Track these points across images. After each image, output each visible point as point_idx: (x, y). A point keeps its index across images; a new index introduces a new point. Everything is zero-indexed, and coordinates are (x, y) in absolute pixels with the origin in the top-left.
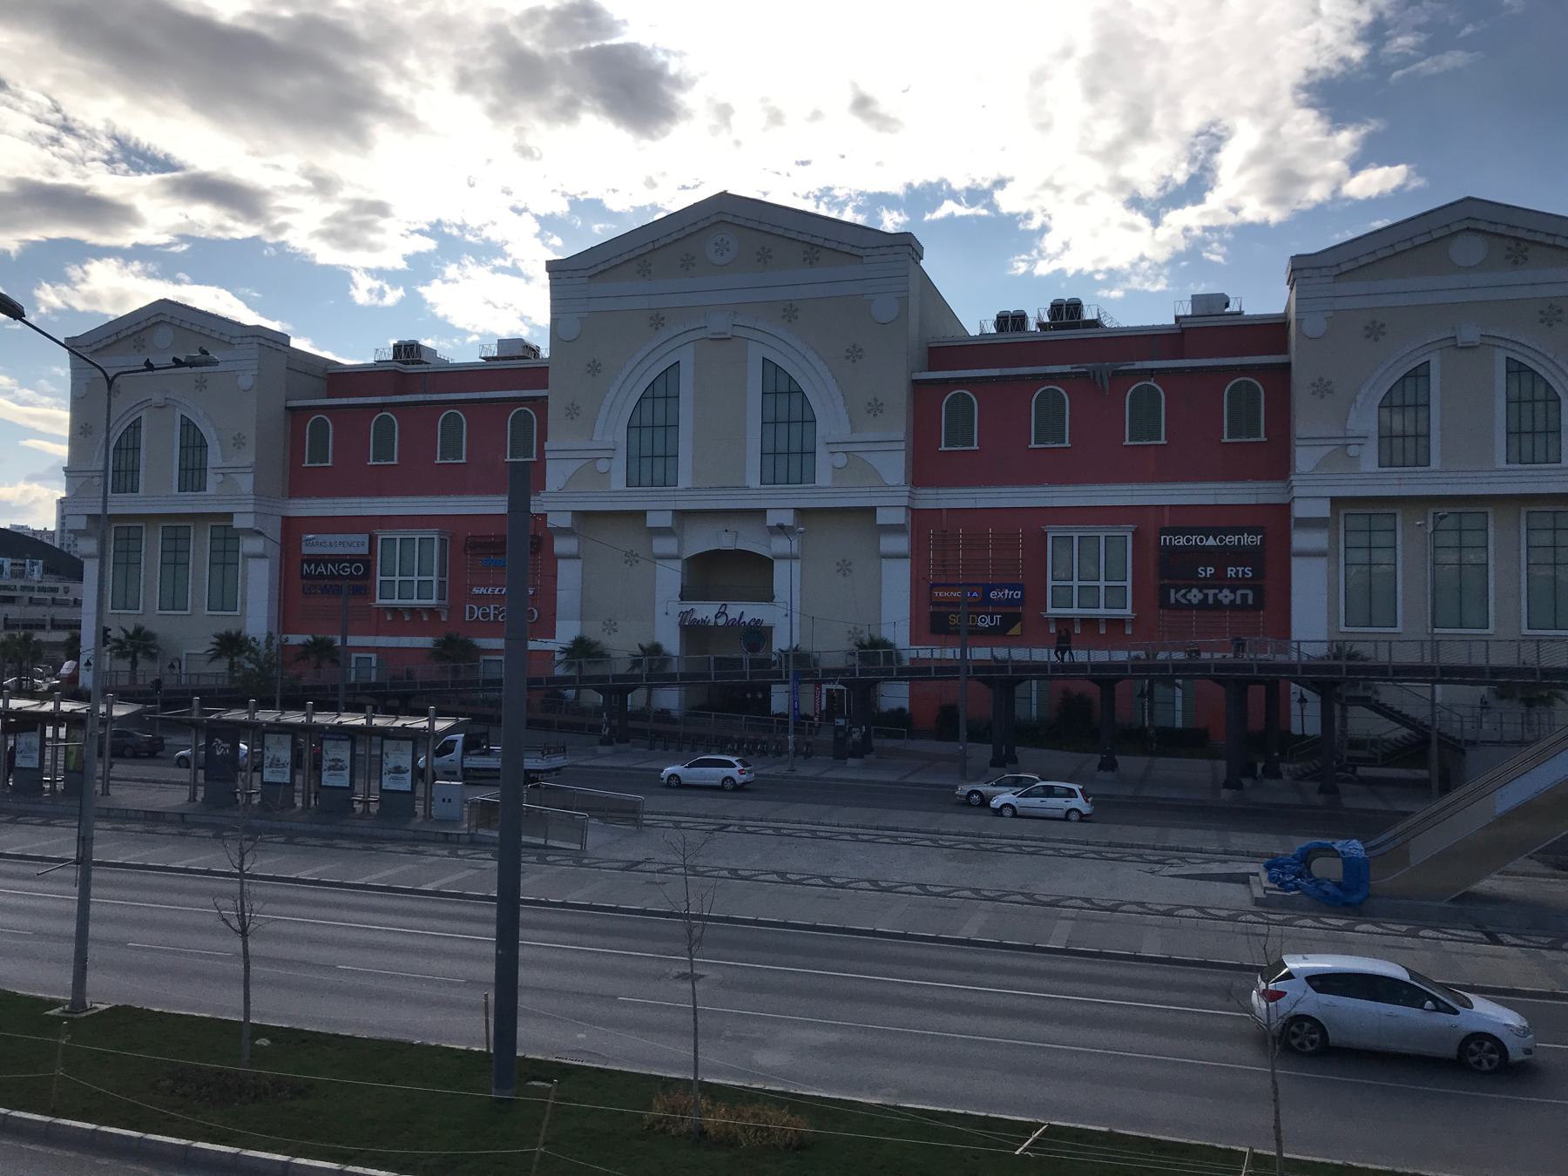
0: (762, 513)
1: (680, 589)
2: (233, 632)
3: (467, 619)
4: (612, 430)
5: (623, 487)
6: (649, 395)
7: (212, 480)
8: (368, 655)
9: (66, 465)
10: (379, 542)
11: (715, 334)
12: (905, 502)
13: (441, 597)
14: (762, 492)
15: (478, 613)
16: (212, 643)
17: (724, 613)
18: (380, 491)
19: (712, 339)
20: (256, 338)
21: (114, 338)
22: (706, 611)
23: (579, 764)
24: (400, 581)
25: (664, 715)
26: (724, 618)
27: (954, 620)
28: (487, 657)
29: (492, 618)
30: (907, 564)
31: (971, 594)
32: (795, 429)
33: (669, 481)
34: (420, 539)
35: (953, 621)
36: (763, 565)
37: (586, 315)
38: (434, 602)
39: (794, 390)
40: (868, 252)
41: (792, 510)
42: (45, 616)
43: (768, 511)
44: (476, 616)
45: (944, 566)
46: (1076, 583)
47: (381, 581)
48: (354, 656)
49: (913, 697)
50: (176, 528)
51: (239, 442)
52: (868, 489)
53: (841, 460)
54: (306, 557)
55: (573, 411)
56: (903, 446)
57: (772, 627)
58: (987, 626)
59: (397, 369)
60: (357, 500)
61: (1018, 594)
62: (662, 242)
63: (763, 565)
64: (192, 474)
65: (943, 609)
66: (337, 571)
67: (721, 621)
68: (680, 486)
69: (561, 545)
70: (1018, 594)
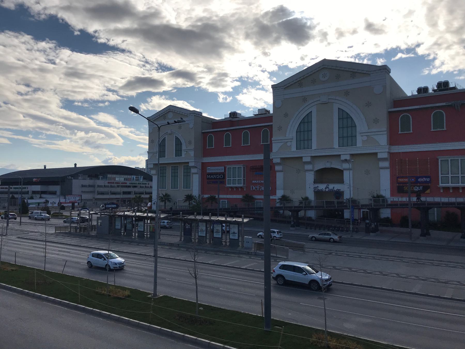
4: (291, 133)
6: (303, 122)
7: (183, 153)
9: (148, 151)
10: (227, 168)
11: (323, 102)
13: (244, 184)
15: (254, 188)
17: (328, 187)
21: (159, 116)
22: (322, 187)
24: (238, 179)
25: (310, 219)
27: (406, 188)
28: (257, 201)
29: (258, 190)
30: (389, 170)
31: (412, 180)
33: (309, 147)
36: (341, 172)
37: (283, 100)
38: (242, 185)
39: (349, 117)
42: (108, 190)
46: (232, 179)
49: (392, 214)
50: (175, 166)
51: (190, 143)
54: (208, 174)
55: (280, 128)
56: (386, 133)
58: (417, 190)
61: (428, 180)
62: (306, 76)
63: (341, 172)
64: (178, 152)
65: (402, 185)
67: (327, 190)
70: (428, 180)
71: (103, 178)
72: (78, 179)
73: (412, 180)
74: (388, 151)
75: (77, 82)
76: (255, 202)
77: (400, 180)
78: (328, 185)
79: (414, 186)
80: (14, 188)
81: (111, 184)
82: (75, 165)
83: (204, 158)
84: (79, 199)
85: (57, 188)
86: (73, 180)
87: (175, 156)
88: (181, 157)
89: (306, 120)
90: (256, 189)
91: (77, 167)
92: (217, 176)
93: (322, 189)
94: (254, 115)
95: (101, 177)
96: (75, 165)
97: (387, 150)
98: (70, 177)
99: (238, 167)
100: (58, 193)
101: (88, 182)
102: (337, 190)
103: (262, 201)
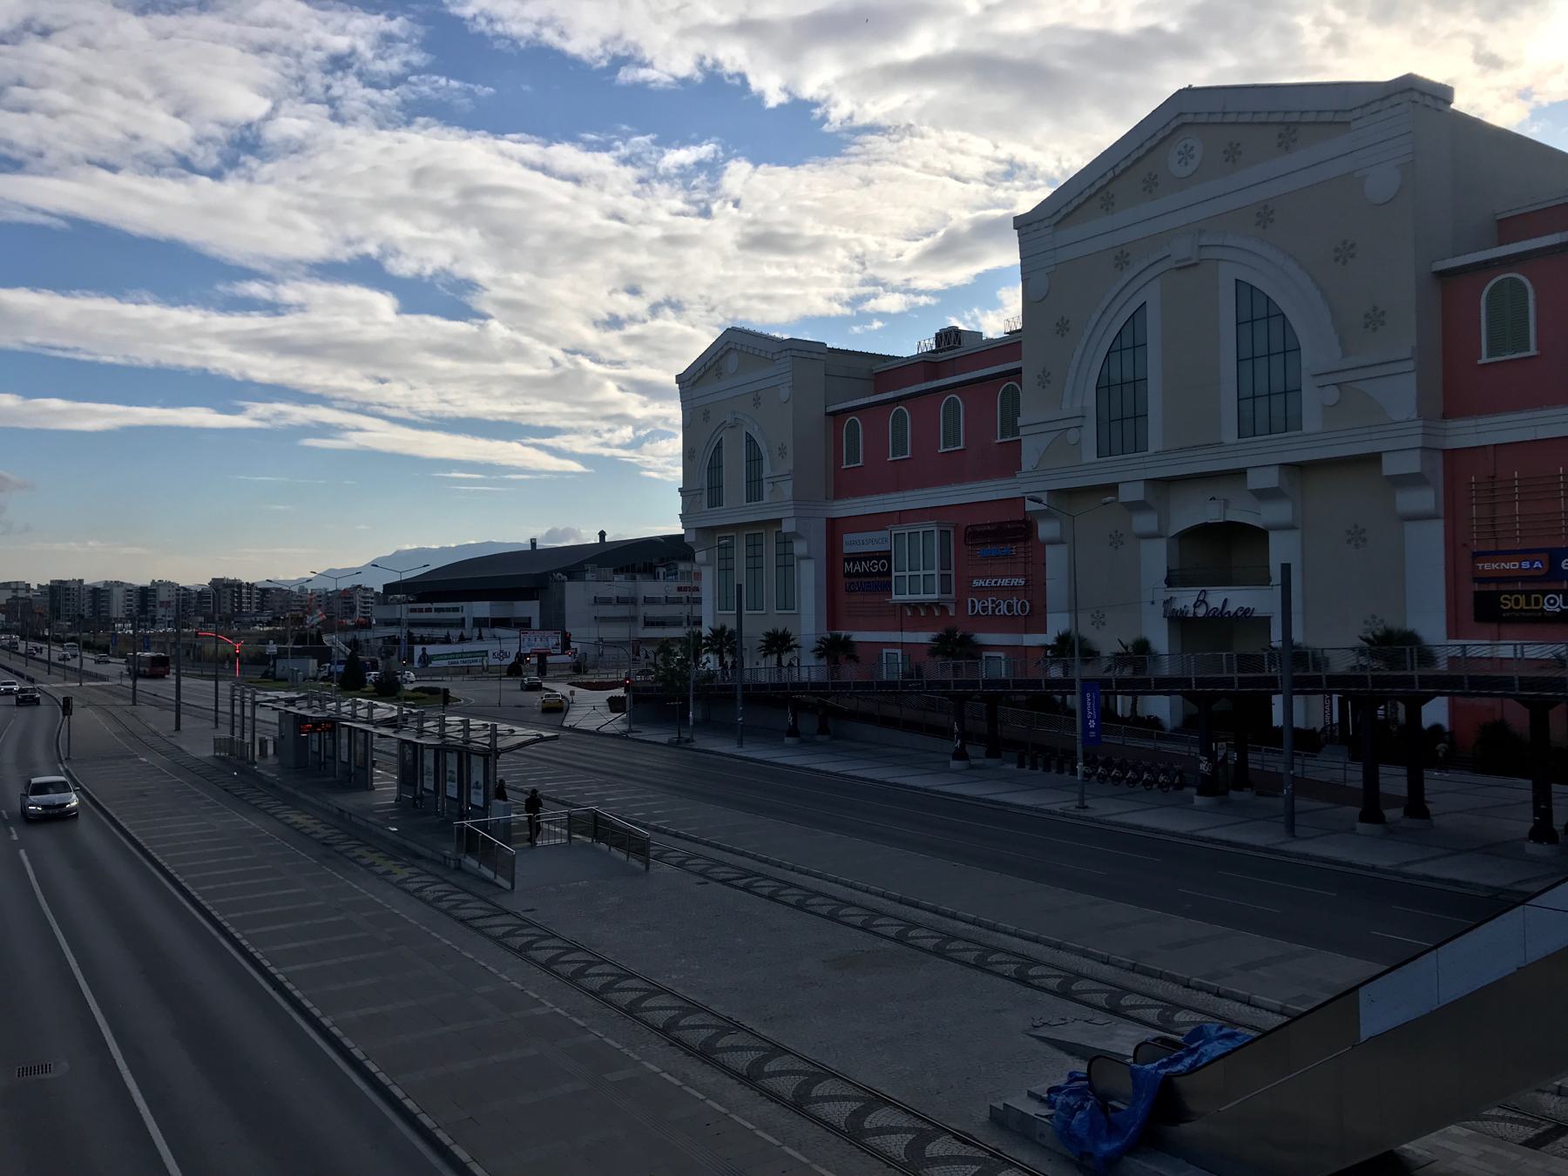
0: (1241, 473)
1: (1165, 574)
2: (780, 631)
3: (970, 613)
5: (1094, 458)
7: (767, 487)
8: (884, 655)
9: (681, 486)
11: (1179, 261)
12: (1418, 441)
13: (945, 589)
14: (1238, 447)
15: (978, 607)
16: (762, 641)
17: (1204, 601)
18: (898, 487)
19: (1177, 268)
20: (788, 351)
21: (703, 370)
22: (1186, 599)
23: (813, 766)
24: (924, 575)
25: (1154, 722)
26: (1204, 606)
27: (1507, 603)
28: (988, 654)
29: (990, 613)
31: (1532, 564)
32: (1277, 361)
33: (1139, 445)
34: (909, 533)
35: (1506, 605)
36: (1257, 537)
38: (936, 596)
39: (1274, 314)
40: (1357, 113)
41: (1046, 493)
42: (681, 613)
43: (1249, 471)
44: (976, 611)
45: (1493, 526)
46: (907, 573)
47: (896, 577)
48: (885, 651)
49: (1453, 711)
50: (755, 531)
52: (1367, 430)
53: (1332, 395)
54: (846, 557)
55: (1044, 379)
57: (1270, 617)
58: (1558, 610)
59: (926, 359)
60: (881, 497)
62: (1122, 166)
63: (1257, 537)
64: (754, 490)
65: (1493, 587)
66: (869, 568)
67: (1201, 612)
68: (1305, 429)
69: (1046, 530)
71: (668, 576)
72: (583, 579)
73: (1535, 566)
74: (1420, 445)
75: (771, 266)
76: (984, 658)
77: (1487, 566)
78: (1203, 593)
79: (1544, 593)
80: (437, 610)
81: (688, 593)
82: (602, 534)
83: (835, 503)
84: (557, 644)
85: (529, 609)
86: (568, 584)
87: (747, 502)
88: (761, 502)
89: (1127, 342)
90: (985, 609)
91: (606, 540)
92: (872, 566)
93: (1183, 608)
94: (1007, 333)
95: (662, 571)
96: (602, 534)
97: (1418, 441)
98: (559, 574)
99: (923, 532)
100: (536, 624)
101: (619, 586)
102: (1240, 614)
103: (1001, 655)
